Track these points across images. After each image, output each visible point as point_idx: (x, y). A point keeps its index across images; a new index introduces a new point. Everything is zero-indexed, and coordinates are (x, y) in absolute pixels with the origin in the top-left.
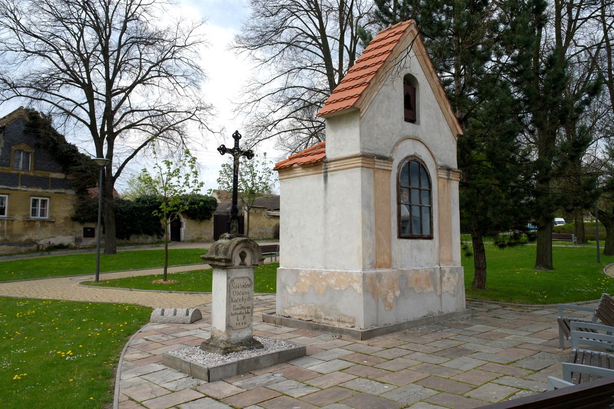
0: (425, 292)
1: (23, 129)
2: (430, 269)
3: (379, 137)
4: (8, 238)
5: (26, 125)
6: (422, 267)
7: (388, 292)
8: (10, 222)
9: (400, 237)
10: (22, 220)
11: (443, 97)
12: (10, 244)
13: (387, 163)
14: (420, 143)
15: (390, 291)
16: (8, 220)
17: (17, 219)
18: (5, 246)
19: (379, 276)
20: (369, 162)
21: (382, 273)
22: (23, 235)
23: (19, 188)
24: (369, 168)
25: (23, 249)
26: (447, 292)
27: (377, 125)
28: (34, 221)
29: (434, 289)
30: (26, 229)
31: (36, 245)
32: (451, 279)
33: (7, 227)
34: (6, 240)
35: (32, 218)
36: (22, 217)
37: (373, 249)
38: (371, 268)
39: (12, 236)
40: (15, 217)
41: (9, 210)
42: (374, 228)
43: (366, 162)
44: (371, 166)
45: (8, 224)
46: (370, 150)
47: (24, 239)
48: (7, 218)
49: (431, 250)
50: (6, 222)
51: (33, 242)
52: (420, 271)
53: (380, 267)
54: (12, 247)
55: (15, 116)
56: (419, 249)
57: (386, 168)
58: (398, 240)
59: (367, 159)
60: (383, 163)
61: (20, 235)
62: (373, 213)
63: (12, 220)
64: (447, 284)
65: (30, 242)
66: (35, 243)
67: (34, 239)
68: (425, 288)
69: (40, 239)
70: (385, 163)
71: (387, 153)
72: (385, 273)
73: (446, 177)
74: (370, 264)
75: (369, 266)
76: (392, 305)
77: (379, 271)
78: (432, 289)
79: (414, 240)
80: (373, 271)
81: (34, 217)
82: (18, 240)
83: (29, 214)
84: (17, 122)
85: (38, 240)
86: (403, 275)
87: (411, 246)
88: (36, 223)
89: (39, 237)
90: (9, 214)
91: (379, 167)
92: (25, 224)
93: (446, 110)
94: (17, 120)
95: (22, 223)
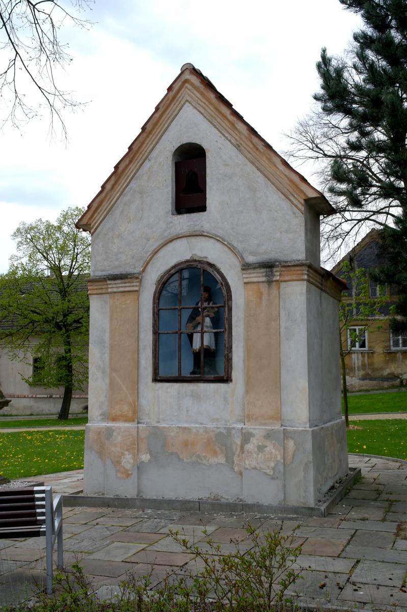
0: (204, 462)
1: (376, 253)
2: (217, 428)
3: (121, 250)
4: (370, 373)
5: (379, 247)
6: (201, 424)
7: (123, 454)
8: (371, 355)
9: (157, 379)
10: (382, 352)
11: (262, 151)
12: (372, 379)
13: (129, 282)
14: (204, 239)
15: (127, 453)
16: (368, 353)
17: (377, 351)
18: (368, 381)
19: (109, 432)
20: (100, 287)
21: (114, 428)
22: (385, 369)
23: (377, 317)
24: (101, 294)
25: (386, 384)
26: (255, 468)
27: (119, 236)
28: (395, 353)
29: (227, 461)
30: (387, 362)
31: (399, 380)
32: (267, 449)
33: (368, 361)
34: (368, 374)
35: (393, 349)
36: (382, 349)
37: (106, 397)
38: (103, 420)
39: (374, 370)
40: (375, 350)
41: (369, 342)
42: (108, 370)
43: (96, 287)
44: (104, 291)
45: (368, 357)
46: (103, 271)
47: (386, 373)
48: (368, 350)
49: (225, 399)
50: (366, 355)
51: (395, 376)
52: (194, 430)
53: (114, 420)
54: (374, 382)
55: (367, 240)
56: (196, 397)
57: (127, 289)
58: (154, 384)
59: (97, 284)
60: (122, 283)
61: (382, 369)
62: (107, 351)
63: (372, 353)
64: (255, 455)
65: (393, 377)
66: (398, 377)
67: (396, 373)
68: (205, 457)
69: (403, 373)
70: (125, 283)
71: (135, 268)
72: (120, 428)
73: (264, 279)
74: (101, 415)
75: (99, 418)
76: (130, 472)
77: (110, 424)
78: (222, 460)
79: (186, 385)
80: (104, 424)
81: (394, 348)
82: (380, 374)
83: (390, 346)
84: (369, 246)
85: (402, 374)
86: (157, 433)
87: (179, 393)
88: (398, 355)
89: (401, 370)
90: (370, 347)
91: (115, 290)
92: (386, 356)
93: (274, 168)
94: (369, 245)
95: (383, 355)
